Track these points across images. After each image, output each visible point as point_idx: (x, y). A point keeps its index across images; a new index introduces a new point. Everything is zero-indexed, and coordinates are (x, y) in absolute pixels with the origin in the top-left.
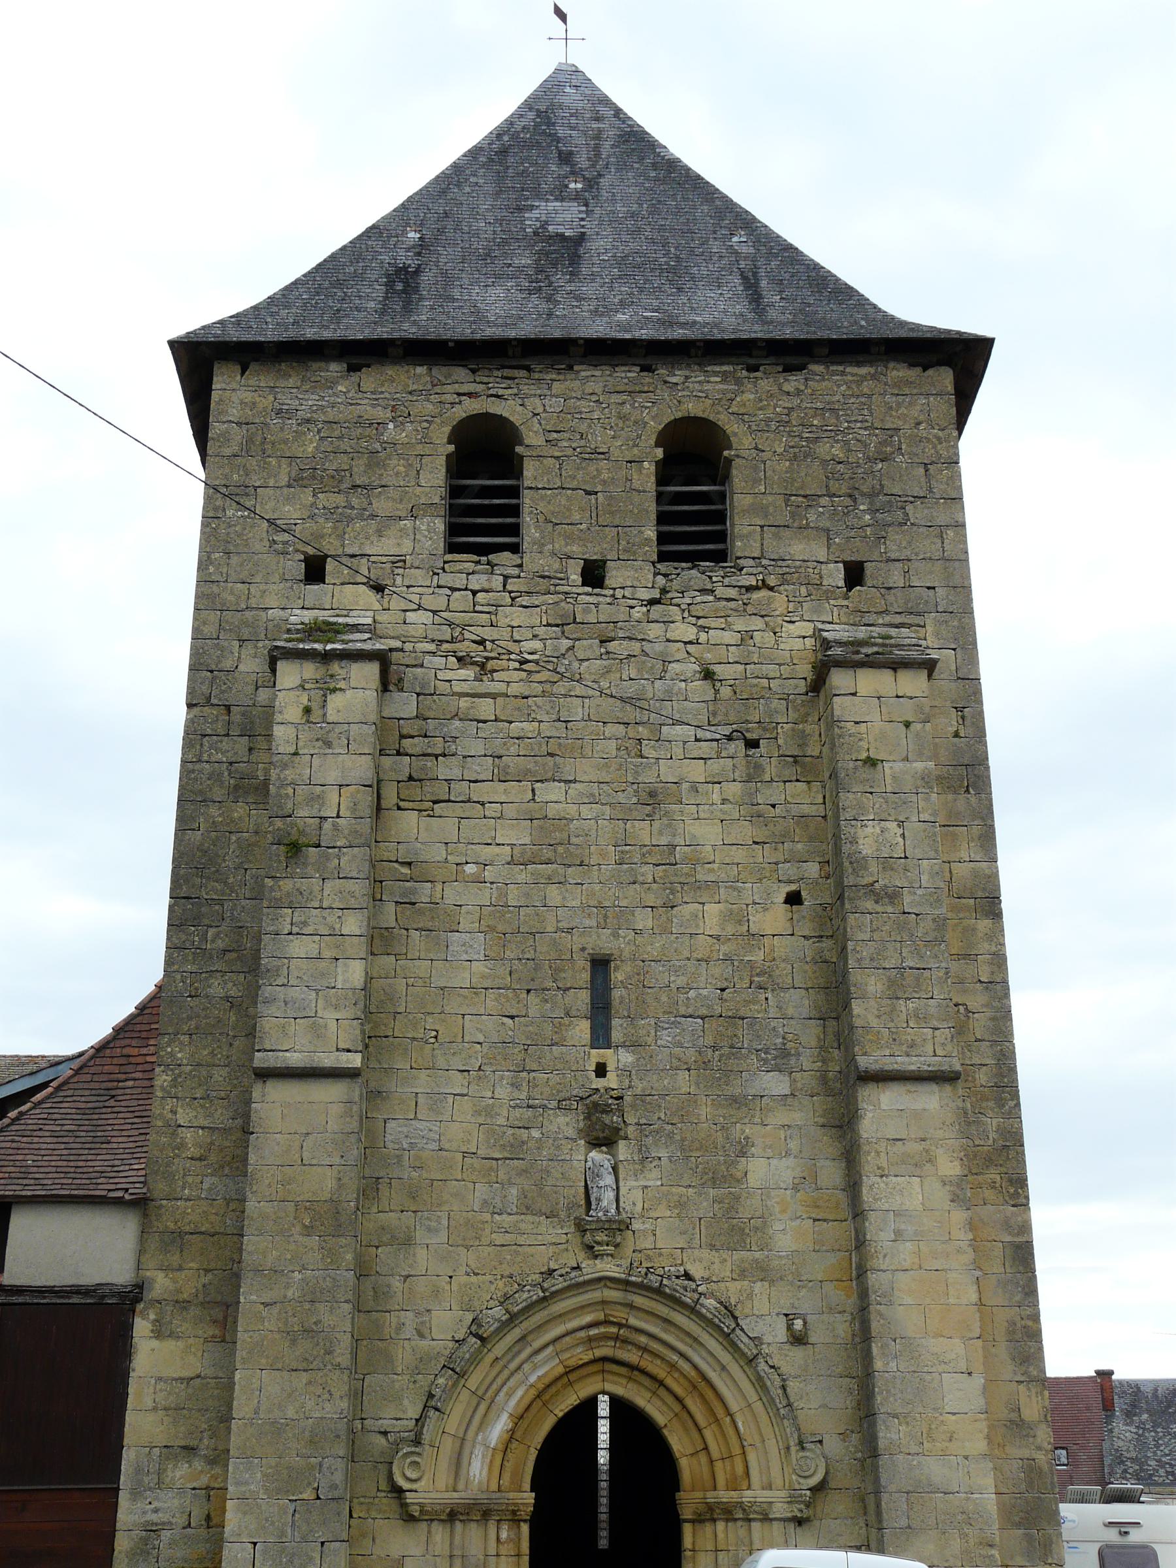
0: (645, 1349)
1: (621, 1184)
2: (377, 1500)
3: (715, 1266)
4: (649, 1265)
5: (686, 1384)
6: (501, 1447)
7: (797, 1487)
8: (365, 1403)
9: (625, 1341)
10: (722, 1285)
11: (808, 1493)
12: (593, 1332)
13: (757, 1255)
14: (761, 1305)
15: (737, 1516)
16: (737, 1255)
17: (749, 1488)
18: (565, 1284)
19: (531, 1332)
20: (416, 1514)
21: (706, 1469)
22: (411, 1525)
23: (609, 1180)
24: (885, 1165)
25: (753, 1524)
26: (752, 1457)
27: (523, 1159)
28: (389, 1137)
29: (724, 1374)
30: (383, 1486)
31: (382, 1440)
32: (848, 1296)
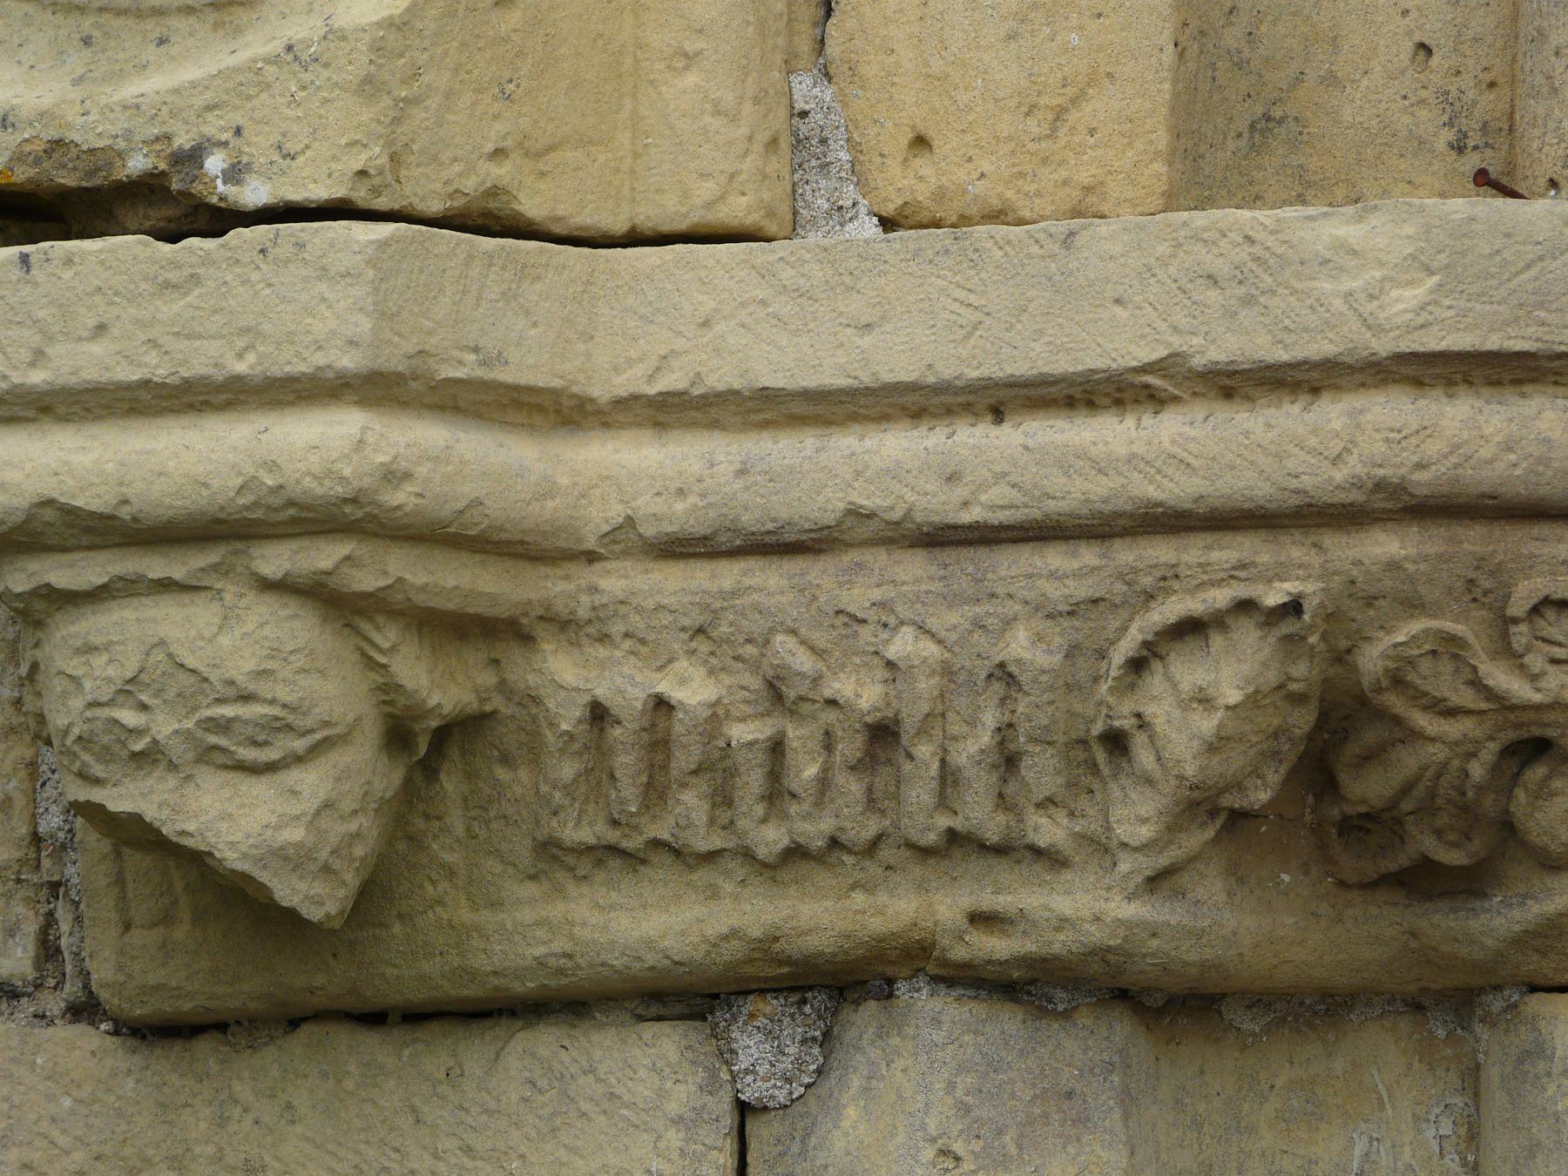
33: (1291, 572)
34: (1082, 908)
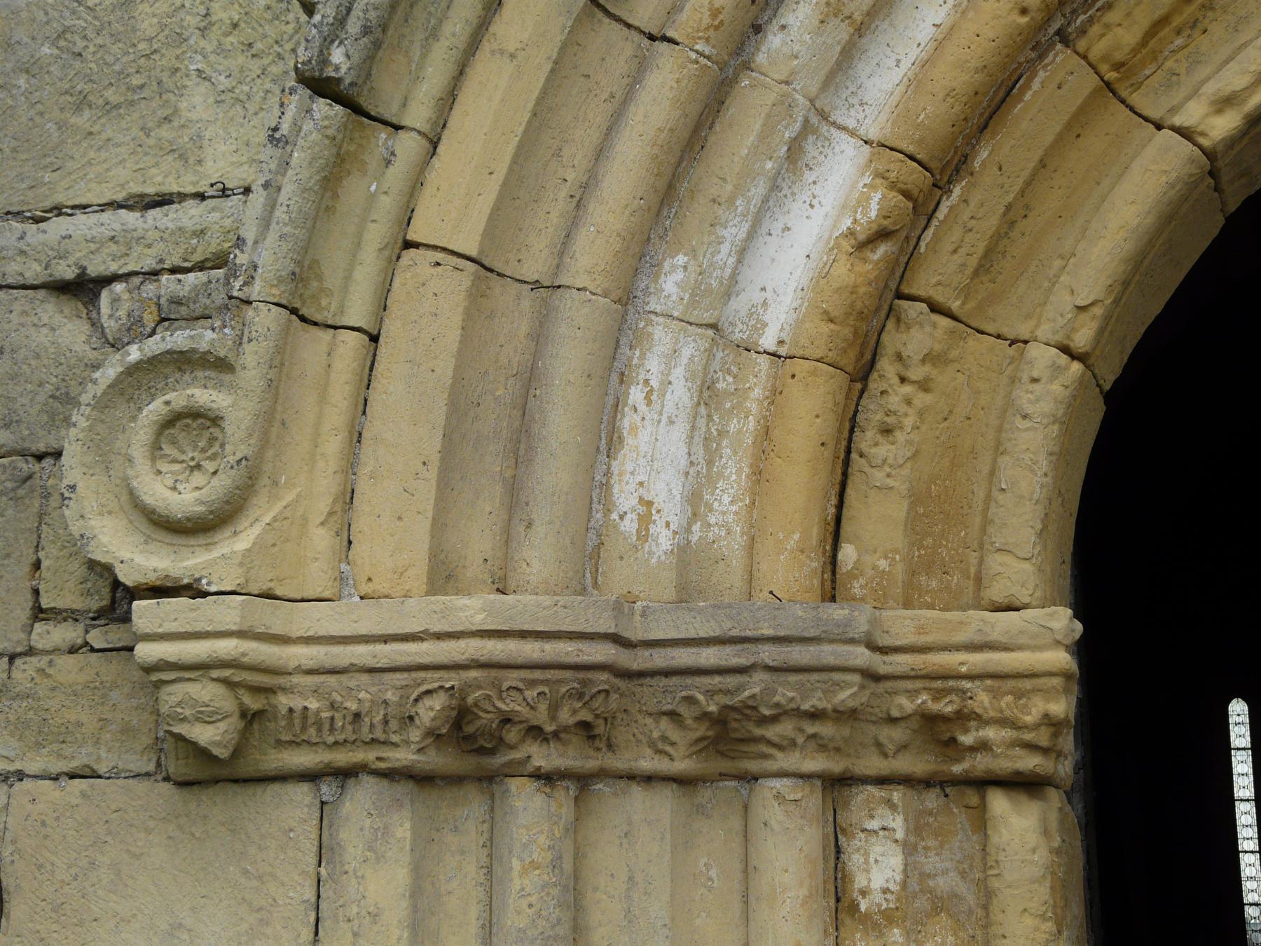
2: (25, 670)
22: (218, 807)
31: (65, 329)
33: (452, 679)
34: (402, 757)
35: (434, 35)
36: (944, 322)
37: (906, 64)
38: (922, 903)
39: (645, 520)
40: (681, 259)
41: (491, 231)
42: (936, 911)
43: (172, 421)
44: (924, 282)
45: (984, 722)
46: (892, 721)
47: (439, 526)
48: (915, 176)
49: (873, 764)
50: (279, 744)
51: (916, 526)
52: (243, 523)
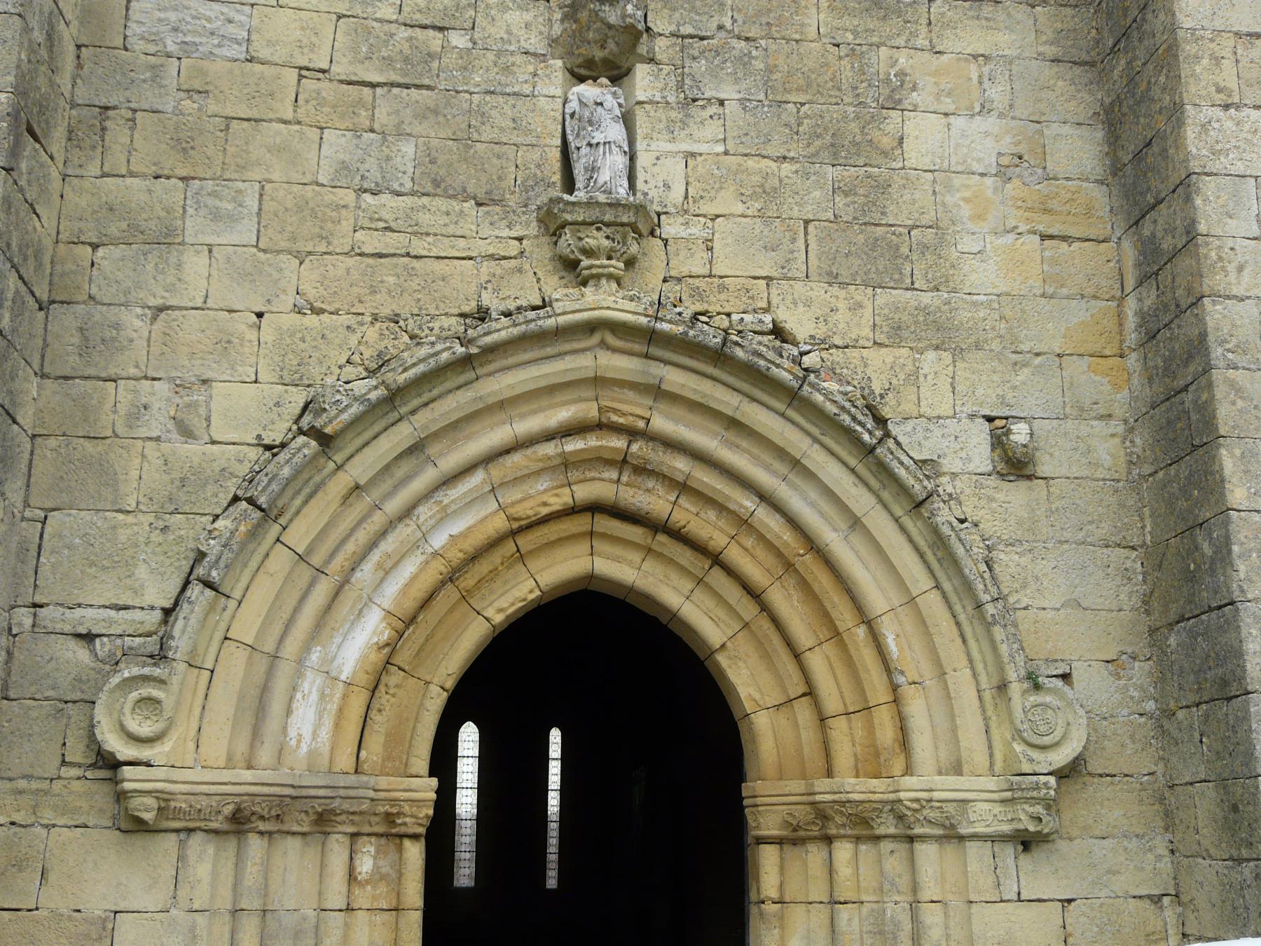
0: (683, 487)
1: (640, 145)
2: (57, 786)
3: (839, 316)
4: (699, 307)
5: (770, 560)
6: (364, 679)
7: (1026, 768)
8: (45, 570)
9: (642, 470)
10: (853, 353)
11: (1052, 780)
12: (573, 445)
13: (926, 298)
14: (936, 399)
15: (881, 831)
16: (883, 297)
17: (908, 770)
18: (515, 331)
19: (436, 435)
20: (148, 816)
21: (809, 735)
22: (139, 841)
23: (616, 132)
24: (1232, 84)
25: (919, 847)
26: (916, 707)
27: (428, 88)
28: (134, 28)
29: (856, 539)
30: (77, 753)
31: (81, 653)
32: (1117, 387)
33: (237, 800)
34: (214, 825)
35: (245, 566)
36: (402, 673)
37: (399, 585)
38: (377, 877)
39: (299, 741)
40: (319, 648)
41: (256, 638)
42: (381, 879)
43: (142, 700)
44: (397, 660)
45: (405, 815)
46: (375, 814)
47: (230, 742)
48: (400, 625)
49: (366, 829)
50: (167, 819)
51: (386, 745)
52: (166, 740)
